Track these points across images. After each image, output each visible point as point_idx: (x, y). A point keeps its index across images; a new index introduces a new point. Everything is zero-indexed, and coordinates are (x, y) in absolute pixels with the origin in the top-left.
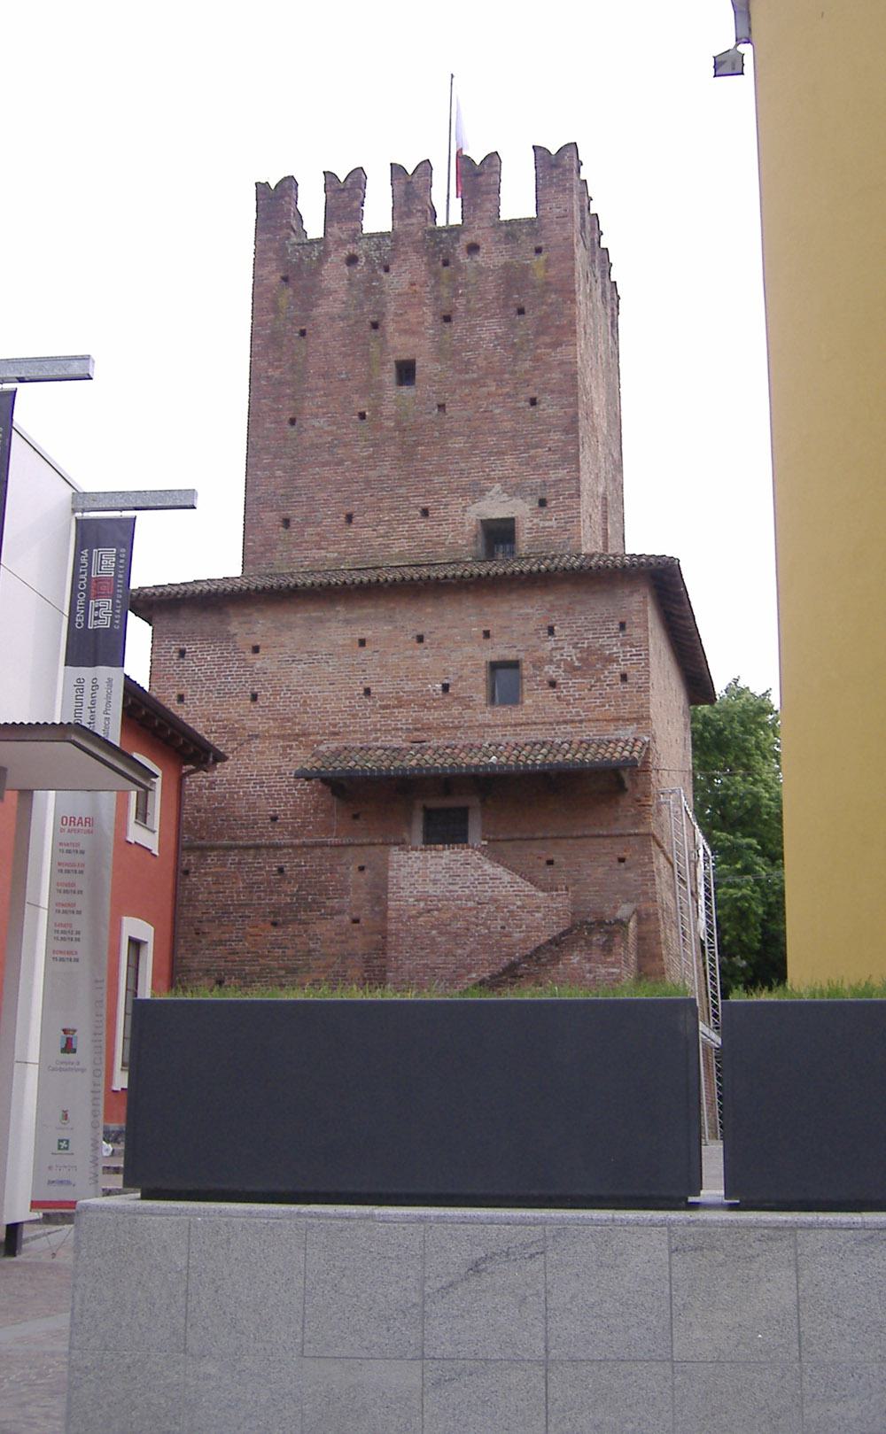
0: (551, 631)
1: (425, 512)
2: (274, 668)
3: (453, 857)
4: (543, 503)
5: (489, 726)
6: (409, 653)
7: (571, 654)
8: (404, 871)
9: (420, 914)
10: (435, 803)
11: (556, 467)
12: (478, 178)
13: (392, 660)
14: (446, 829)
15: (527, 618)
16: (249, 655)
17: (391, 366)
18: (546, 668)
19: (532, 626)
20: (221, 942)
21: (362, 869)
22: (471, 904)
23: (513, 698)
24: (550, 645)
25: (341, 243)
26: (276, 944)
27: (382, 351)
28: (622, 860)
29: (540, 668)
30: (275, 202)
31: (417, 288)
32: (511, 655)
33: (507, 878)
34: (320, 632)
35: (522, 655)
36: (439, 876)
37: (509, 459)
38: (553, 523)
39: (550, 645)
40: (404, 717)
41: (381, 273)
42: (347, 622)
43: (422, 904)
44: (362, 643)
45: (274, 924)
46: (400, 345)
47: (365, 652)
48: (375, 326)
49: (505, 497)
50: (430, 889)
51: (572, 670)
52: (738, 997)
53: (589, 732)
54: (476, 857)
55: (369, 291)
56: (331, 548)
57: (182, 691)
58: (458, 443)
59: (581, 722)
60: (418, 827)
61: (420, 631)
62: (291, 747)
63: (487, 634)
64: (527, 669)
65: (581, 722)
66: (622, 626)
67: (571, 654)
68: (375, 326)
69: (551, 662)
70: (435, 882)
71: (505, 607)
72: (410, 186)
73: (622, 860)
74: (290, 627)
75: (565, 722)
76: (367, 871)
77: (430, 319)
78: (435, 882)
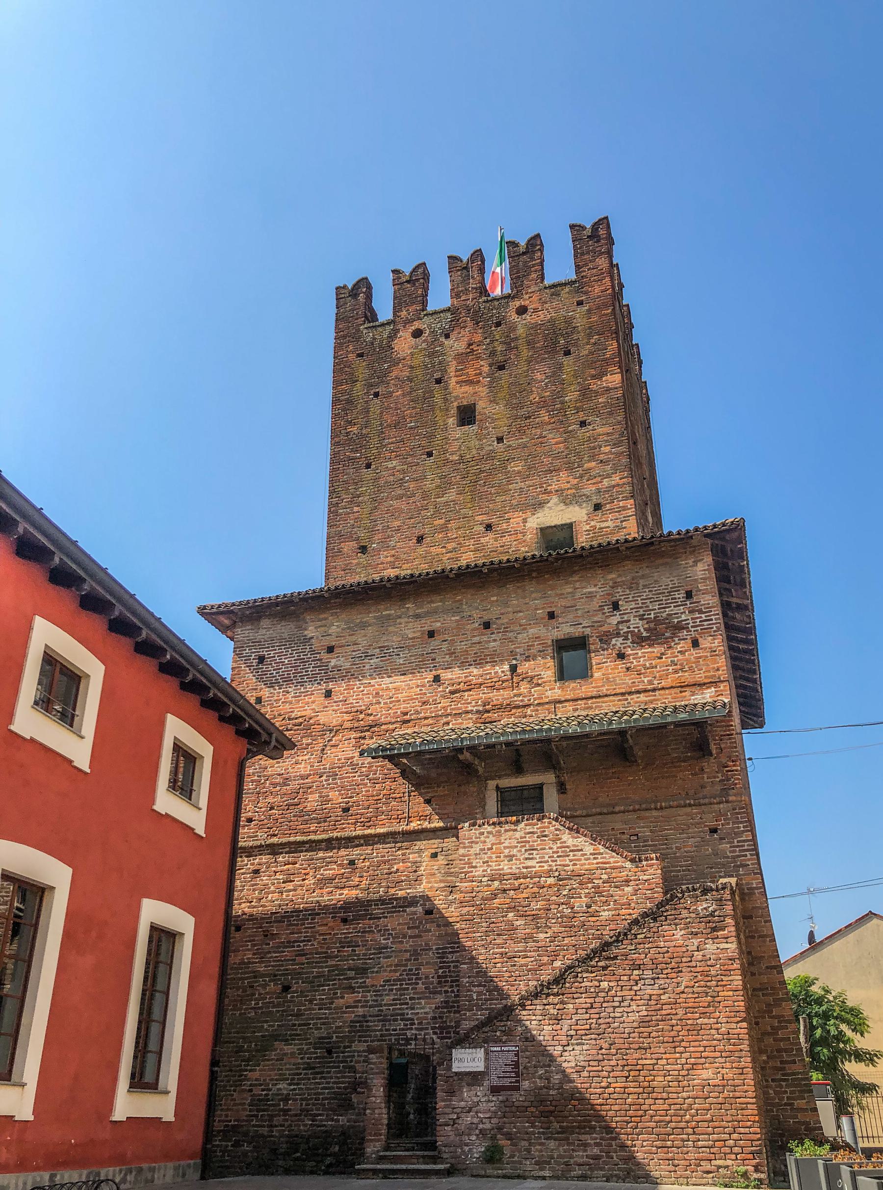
0: (616, 606)
1: (489, 527)
2: (347, 665)
3: (529, 829)
4: (597, 507)
5: (560, 702)
6: (476, 639)
7: (637, 625)
8: (477, 848)
9: (495, 896)
10: (507, 782)
11: (608, 476)
12: (526, 256)
13: (460, 647)
14: (522, 804)
15: (591, 596)
16: (324, 656)
17: (454, 411)
18: (614, 641)
19: (595, 604)
20: (290, 944)
21: (434, 855)
22: (551, 881)
23: (584, 673)
24: (614, 620)
25: (408, 322)
26: (344, 943)
27: (446, 400)
28: (714, 831)
29: (607, 642)
30: (354, 299)
31: (474, 347)
32: (577, 631)
33: (589, 849)
34: (391, 629)
35: (588, 631)
36: (515, 851)
37: (563, 475)
38: (610, 523)
39: (614, 620)
40: (473, 700)
41: (443, 339)
42: (417, 616)
43: (496, 883)
44: (431, 634)
45: (345, 921)
46: (461, 393)
47: (434, 643)
48: (438, 381)
49: (562, 506)
50: (506, 867)
51: (639, 641)
52: (820, 1162)
53: (665, 700)
54: (551, 827)
55: (432, 355)
56: (404, 567)
57: (260, 694)
58: (516, 467)
59: (654, 690)
60: (492, 803)
61: (486, 619)
62: (364, 738)
63: (551, 616)
64: (594, 643)
65: (654, 690)
66: (689, 595)
67: (637, 625)
68: (438, 381)
69: (618, 635)
70: (510, 857)
71: (568, 589)
72: (467, 269)
73: (714, 831)
74: (363, 626)
75: (638, 692)
76: (440, 857)
77: (486, 369)
78: (510, 857)
